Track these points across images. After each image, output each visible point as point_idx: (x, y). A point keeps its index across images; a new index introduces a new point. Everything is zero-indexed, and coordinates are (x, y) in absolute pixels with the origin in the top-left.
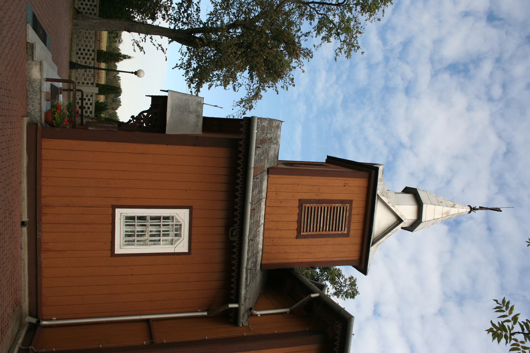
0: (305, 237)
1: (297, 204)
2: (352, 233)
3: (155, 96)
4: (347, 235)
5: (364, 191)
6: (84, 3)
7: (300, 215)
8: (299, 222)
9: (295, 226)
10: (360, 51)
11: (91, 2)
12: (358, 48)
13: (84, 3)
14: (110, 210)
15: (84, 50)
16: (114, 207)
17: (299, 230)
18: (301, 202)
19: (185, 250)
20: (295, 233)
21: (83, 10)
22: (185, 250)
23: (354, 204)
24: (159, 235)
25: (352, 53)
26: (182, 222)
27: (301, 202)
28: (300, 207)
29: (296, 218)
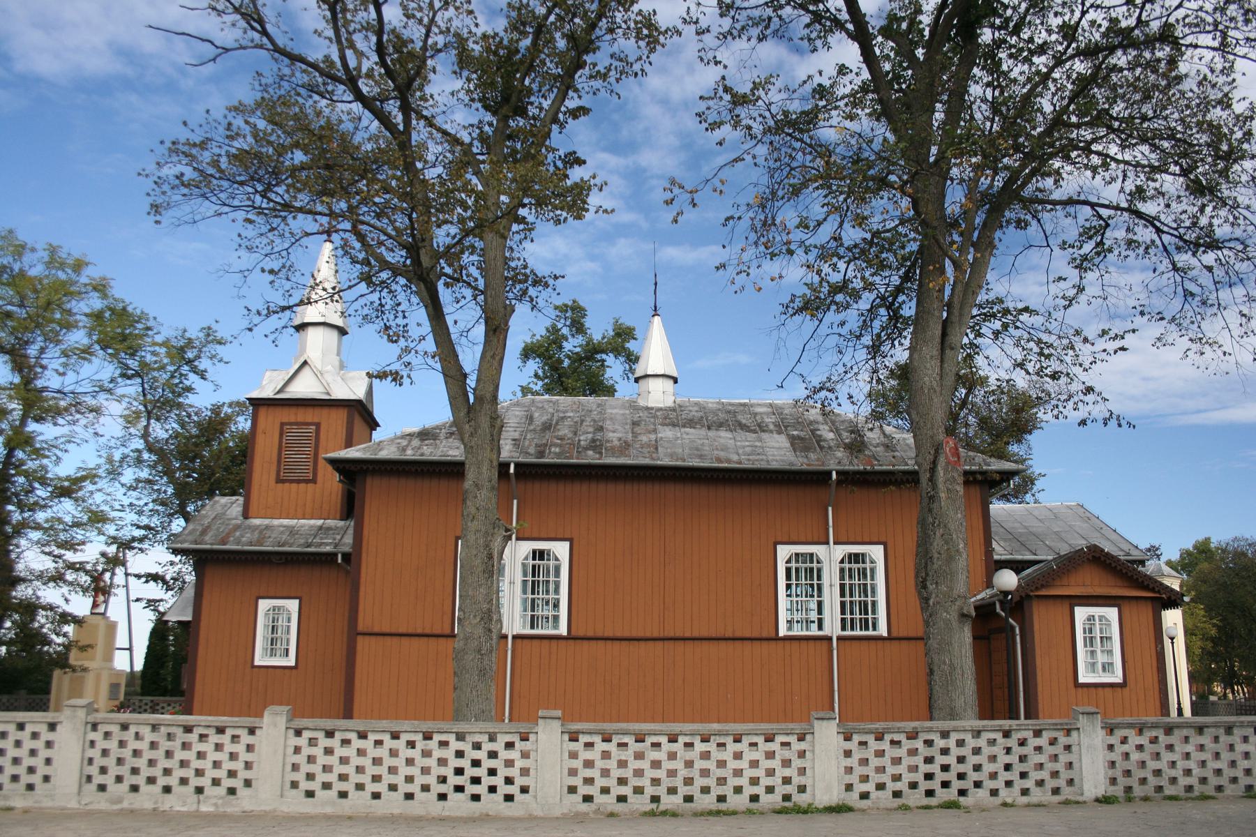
0: (315, 474)
1: (280, 485)
2: (316, 420)
3: (146, 658)
4: (318, 425)
5: (271, 409)
6: (12, 752)
7: (292, 481)
8: (298, 482)
9: (302, 485)
10: (215, 326)
11: (7, 744)
12: (209, 328)
13: (12, 752)
14: (255, 670)
15: (492, 772)
16: (253, 667)
17: (307, 481)
18: (279, 480)
19: (567, 545)
20: (310, 485)
21: (123, 765)
22: (567, 545)
23: (285, 420)
24: (548, 582)
25: (219, 335)
26: (271, 606)
27: (279, 480)
28: (283, 481)
29: (294, 486)
